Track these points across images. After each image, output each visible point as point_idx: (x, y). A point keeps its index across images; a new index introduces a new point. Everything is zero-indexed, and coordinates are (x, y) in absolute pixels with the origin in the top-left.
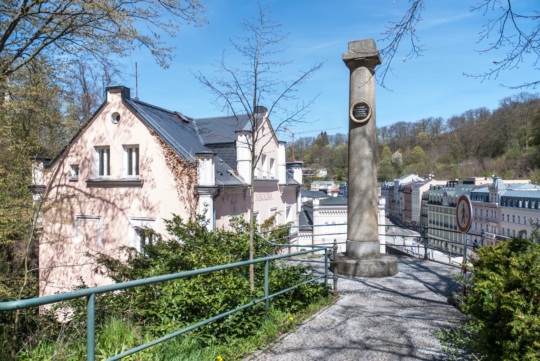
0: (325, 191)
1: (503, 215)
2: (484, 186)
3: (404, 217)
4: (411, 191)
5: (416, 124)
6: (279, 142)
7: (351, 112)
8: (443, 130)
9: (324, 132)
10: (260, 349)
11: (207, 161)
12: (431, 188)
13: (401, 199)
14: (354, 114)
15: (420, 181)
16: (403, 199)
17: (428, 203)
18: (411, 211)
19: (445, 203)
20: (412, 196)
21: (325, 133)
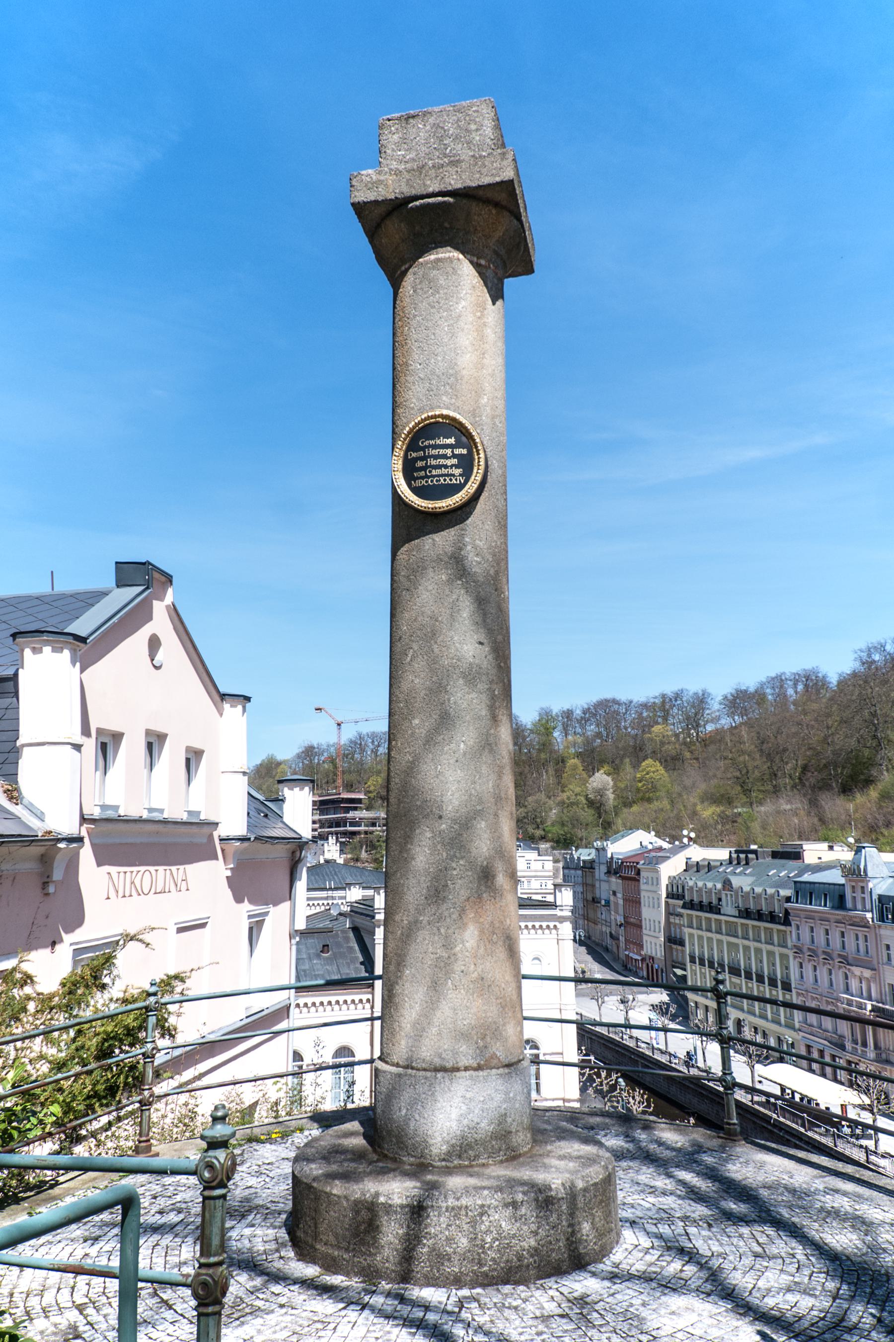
3: (622, 945)
4: (638, 873)
13: (614, 893)
15: (660, 849)
16: (619, 895)
19: (728, 908)
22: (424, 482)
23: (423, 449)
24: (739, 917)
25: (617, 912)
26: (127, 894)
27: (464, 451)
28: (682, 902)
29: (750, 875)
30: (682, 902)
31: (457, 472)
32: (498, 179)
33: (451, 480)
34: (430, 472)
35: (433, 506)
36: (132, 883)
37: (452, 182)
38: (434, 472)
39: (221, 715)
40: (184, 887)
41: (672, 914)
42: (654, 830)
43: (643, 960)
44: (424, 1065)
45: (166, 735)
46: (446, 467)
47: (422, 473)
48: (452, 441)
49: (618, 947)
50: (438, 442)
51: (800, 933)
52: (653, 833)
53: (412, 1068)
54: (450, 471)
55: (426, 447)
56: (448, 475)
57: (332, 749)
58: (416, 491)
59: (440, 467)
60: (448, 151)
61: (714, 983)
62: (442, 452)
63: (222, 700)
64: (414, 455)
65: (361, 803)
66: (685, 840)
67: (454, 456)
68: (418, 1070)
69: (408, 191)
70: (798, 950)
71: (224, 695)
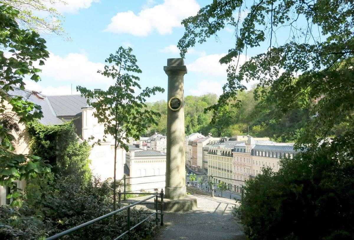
2: (242, 142)
3: (192, 163)
4: (197, 145)
7: (169, 104)
10: (123, 131)
11: (47, 61)
13: (190, 150)
15: (203, 138)
16: (192, 150)
17: (208, 153)
18: (197, 159)
19: (219, 153)
25: (191, 155)
29: (225, 145)
39: (9, 51)
43: (197, 167)
70: (234, 163)
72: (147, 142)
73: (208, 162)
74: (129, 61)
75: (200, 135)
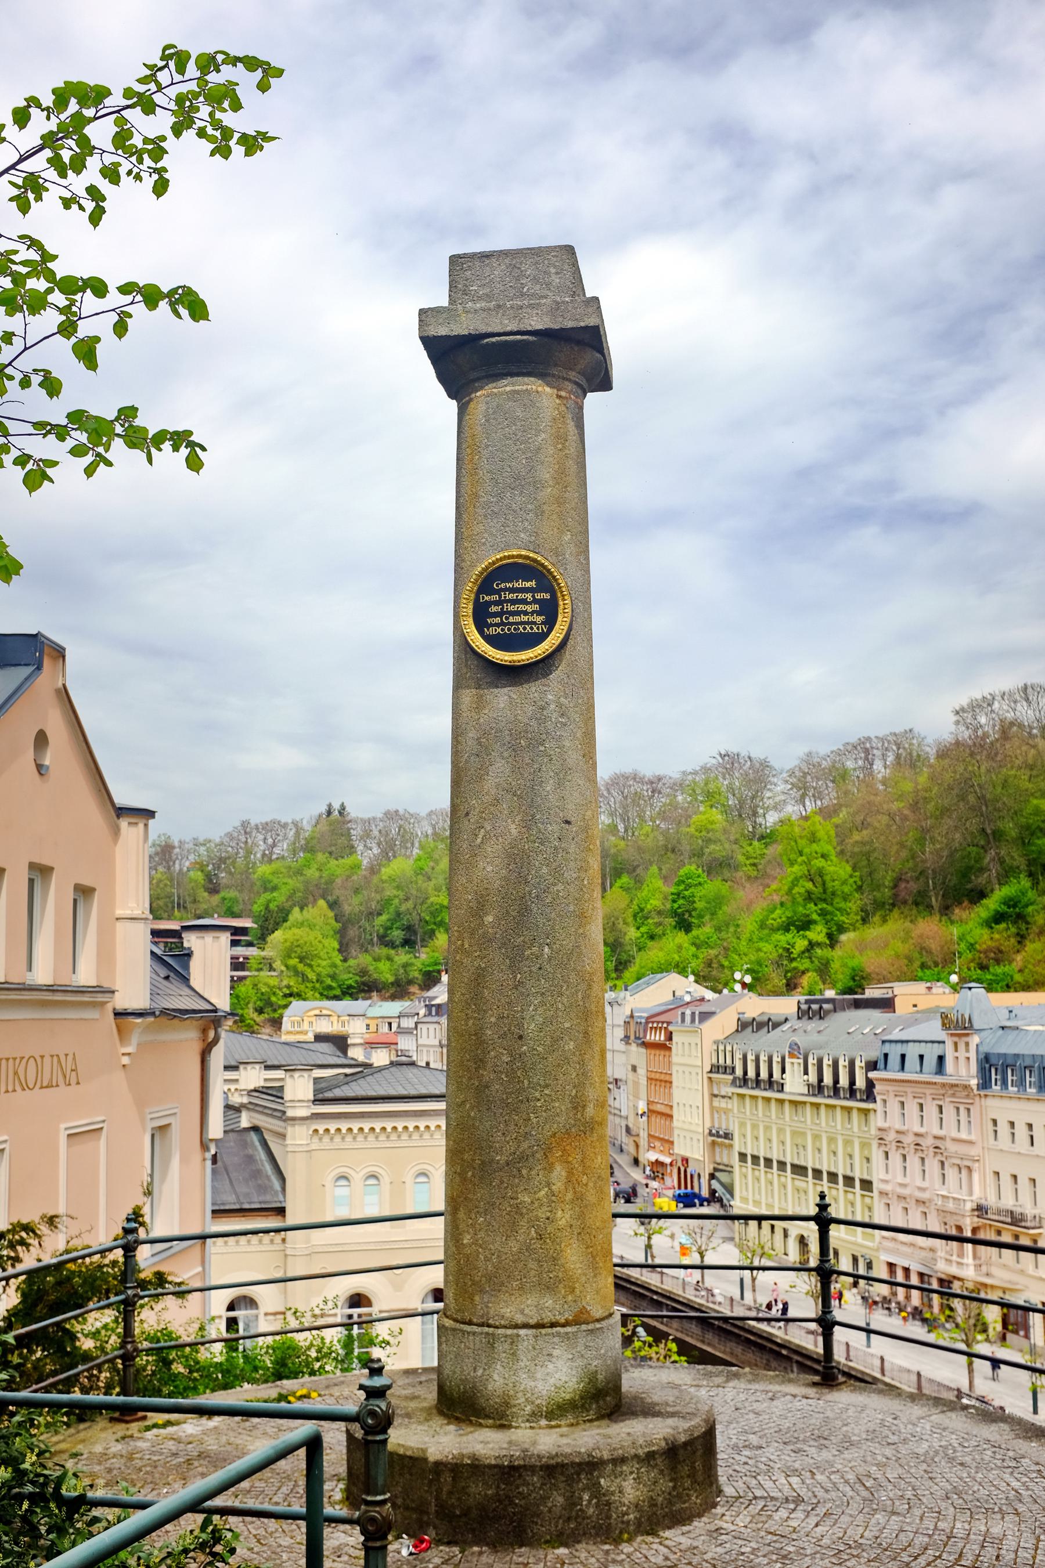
0: (340, 1042)
1: (995, 1122)
3: (643, 1142)
5: (679, 786)
6: (122, 812)
8: (775, 808)
9: (336, 806)
12: (744, 1025)
13: (634, 1069)
14: (481, 624)
16: (642, 1071)
20: (675, 1059)
21: (343, 807)
22: (499, 630)
23: (498, 592)
24: (808, 1095)
26: (10, 1089)
27: (547, 596)
28: (731, 1077)
30: (731, 1077)
31: (539, 619)
32: (582, 324)
33: (532, 629)
34: (507, 618)
35: (510, 659)
36: (16, 1073)
37: (533, 323)
38: (511, 619)
40: (73, 1081)
41: (716, 1096)
42: (693, 973)
44: (503, 1322)
45: (52, 869)
46: (526, 613)
47: (498, 620)
48: (532, 584)
49: (637, 1146)
50: (516, 585)
51: (888, 1114)
52: (692, 978)
53: (489, 1326)
54: (531, 619)
55: (502, 590)
56: (528, 623)
57: (202, 850)
58: (493, 641)
59: (518, 613)
60: (525, 290)
61: (817, 1209)
62: (521, 596)
63: (118, 817)
64: (487, 598)
65: (246, 935)
66: (738, 987)
67: (535, 601)
68: (497, 1327)
69: (483, 329)
71: (120, 809)
72: (394, 1026)
73: (736, 1137)
74: (82, 208)
75: (686, 987)
